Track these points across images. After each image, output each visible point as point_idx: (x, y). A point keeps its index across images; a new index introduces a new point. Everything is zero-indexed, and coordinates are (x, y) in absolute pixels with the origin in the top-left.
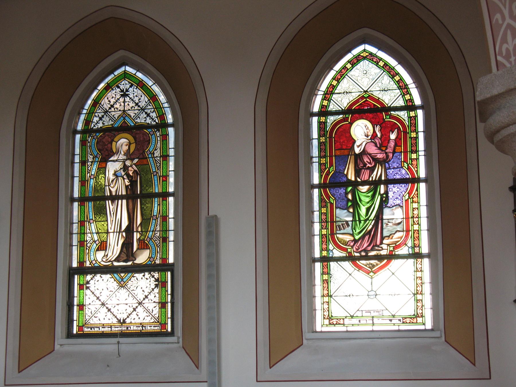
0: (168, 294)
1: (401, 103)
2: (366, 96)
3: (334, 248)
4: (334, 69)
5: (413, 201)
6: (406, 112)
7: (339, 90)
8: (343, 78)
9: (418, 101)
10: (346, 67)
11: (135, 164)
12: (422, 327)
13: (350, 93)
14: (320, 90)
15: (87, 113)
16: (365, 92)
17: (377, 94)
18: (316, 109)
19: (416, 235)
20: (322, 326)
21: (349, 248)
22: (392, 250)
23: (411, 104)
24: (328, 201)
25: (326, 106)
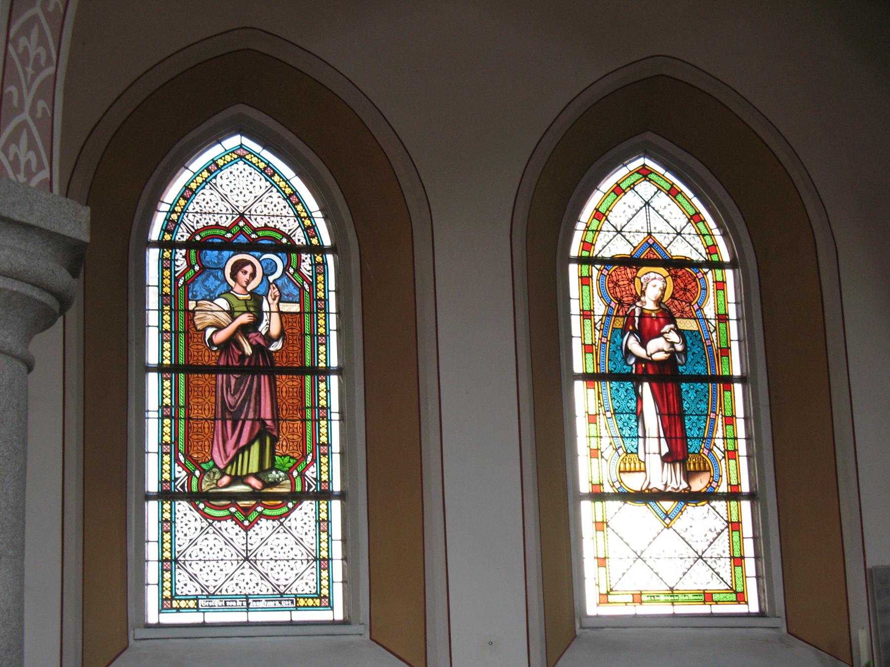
11: (281, 314)
14: (165, 201)
15: (169, 211)
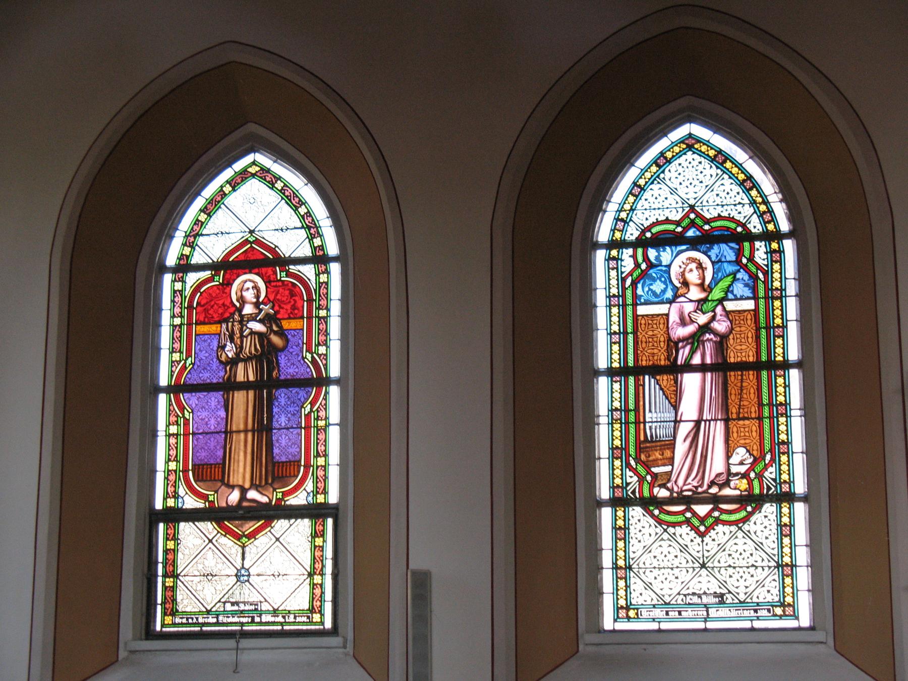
0: (163, 563)
1: (306, 251)
2: (252, 240)
3: (305, 489)
4: (636, 165)
5: (318, 416)
6: (313, 266)
7: (210, 229)
8: (218, 209)
9: (333, 249)
10: (282, 189)
12: (791, 624)
13: (277, 230)
16: (251, 232)
17: (271, 238)
18: (171, 260)
19: (321, 473)
20: (615, 621)
21: (277, 495)
22: (281, 497)
23: (321, 253)
24: (181, 416)
25: (187, 257)
